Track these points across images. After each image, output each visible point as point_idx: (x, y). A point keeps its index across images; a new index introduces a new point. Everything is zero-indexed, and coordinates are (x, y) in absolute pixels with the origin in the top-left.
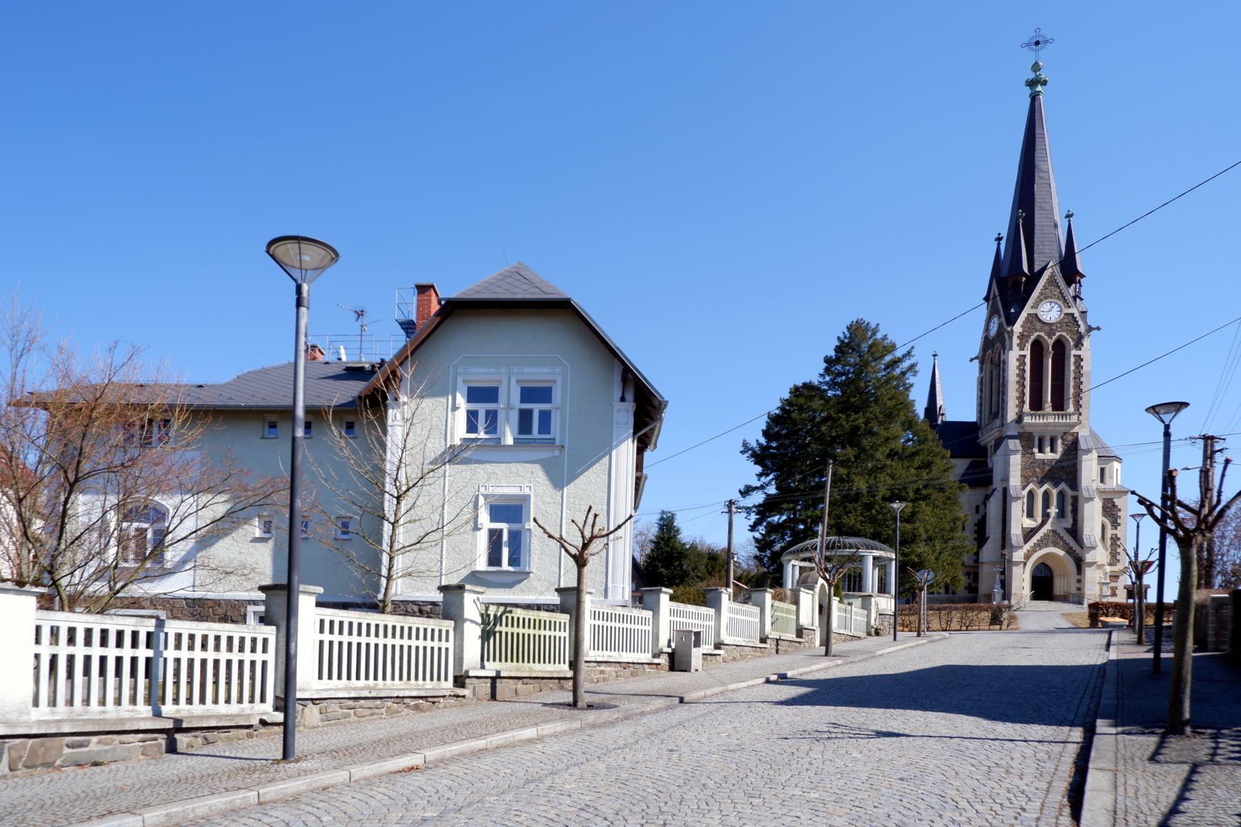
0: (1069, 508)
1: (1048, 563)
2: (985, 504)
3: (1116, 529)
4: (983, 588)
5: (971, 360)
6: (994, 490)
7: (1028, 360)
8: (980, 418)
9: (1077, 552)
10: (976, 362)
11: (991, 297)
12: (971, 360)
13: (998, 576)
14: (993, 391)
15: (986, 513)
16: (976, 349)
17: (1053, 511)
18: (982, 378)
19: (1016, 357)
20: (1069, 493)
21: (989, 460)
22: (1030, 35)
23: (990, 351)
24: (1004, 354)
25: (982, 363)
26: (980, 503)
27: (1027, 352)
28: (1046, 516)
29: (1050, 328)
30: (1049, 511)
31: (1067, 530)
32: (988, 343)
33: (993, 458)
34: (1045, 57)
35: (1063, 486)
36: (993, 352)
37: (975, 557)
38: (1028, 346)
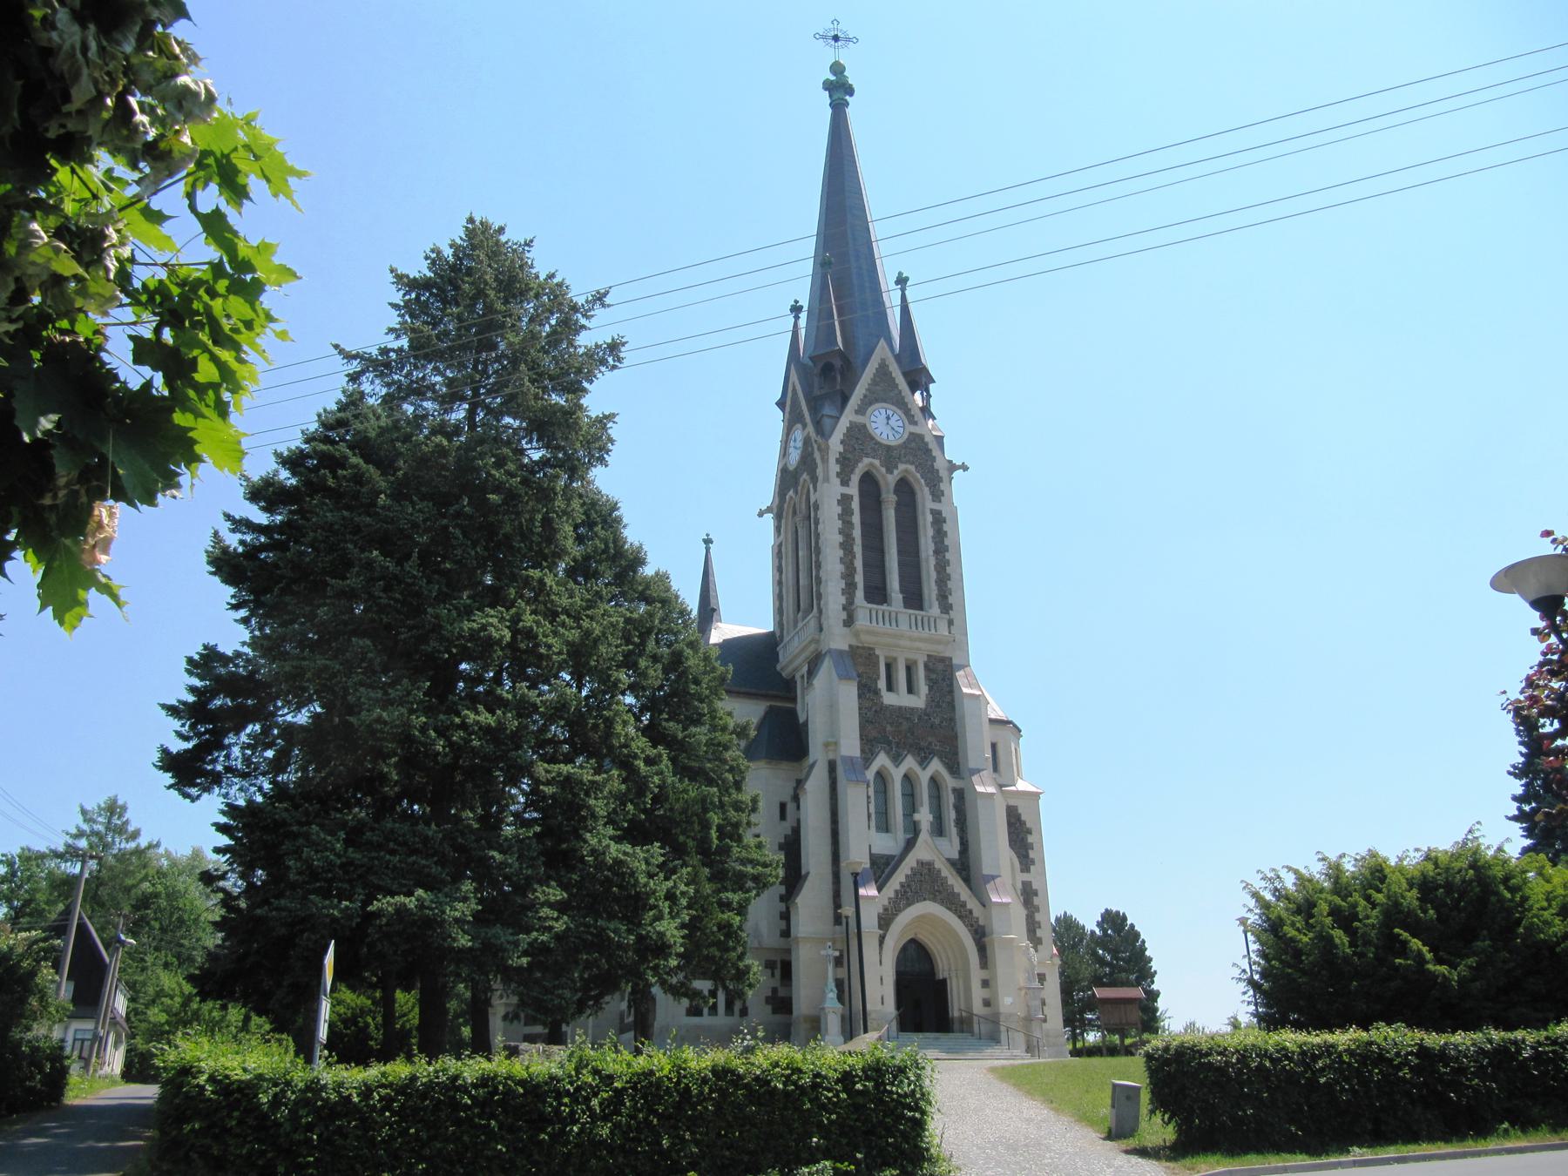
0: (950, 815)
1: (925, 938)
2: (796, 799)
3: (1028, 870)
4: (802, 1002)
5: (761, 514)
6: (812, 766)
7: (855, 505)
8: (780, 623)
9: (976, 914)
10: (769, 517)
11: (788, 403)
12: (761, 514)
13: (830, 968)
14: (801, 567)
15: (799, 821)
16: (767, 495)
17: (924, 816)
18: (780, 546)
19: (831, 493)
20: (950, 782)
21: (799, 707)
22: (824, 26)
23: (791, 493)
24: (815, 490)
25: (779, 517)
26: (787, 798)
27: (853, 490)
28: (914, 830)
29: (890, 455)
30: (917, 817)
31: (952, 862)
32: (788, 479)
33: (807, 698)
34: (845, 56)
35: (936, 766)
36: (796, 492)
37: (783, 923)
38: (855, 479)
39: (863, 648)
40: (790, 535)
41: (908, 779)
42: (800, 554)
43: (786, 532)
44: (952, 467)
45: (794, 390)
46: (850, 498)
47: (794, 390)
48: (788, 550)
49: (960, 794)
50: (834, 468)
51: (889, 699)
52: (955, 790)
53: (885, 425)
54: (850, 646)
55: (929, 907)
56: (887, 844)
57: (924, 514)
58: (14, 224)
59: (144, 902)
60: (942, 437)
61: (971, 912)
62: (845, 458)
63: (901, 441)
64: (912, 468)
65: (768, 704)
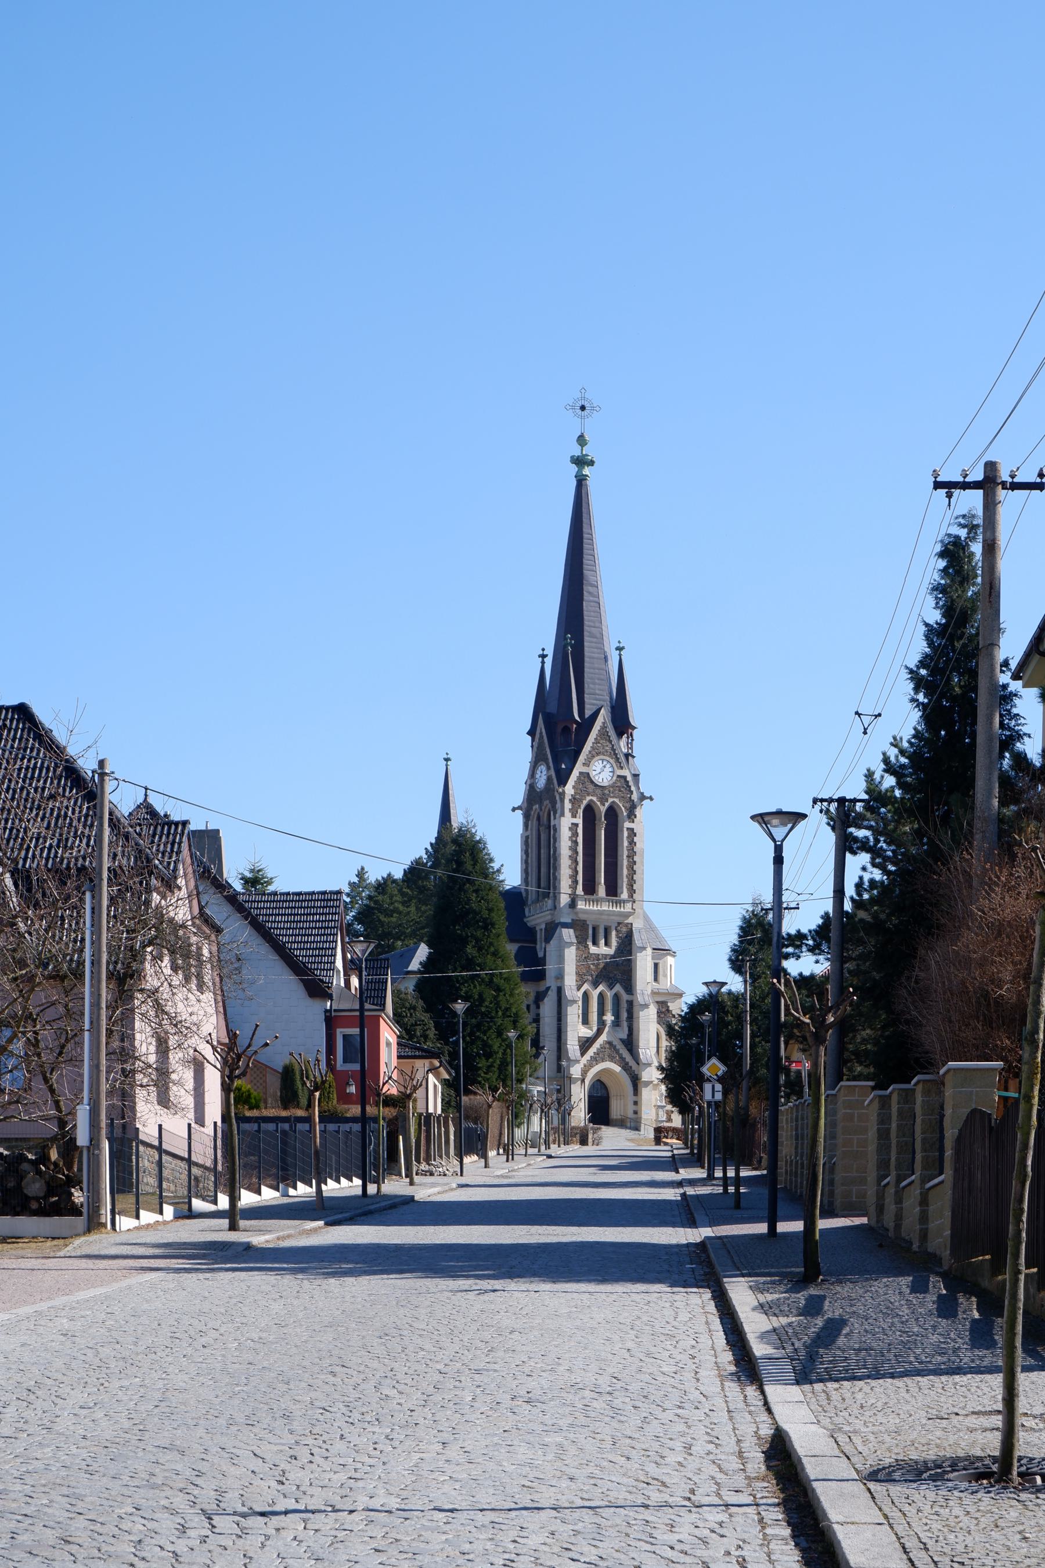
0: (624, 1015)
5: (514, 809)
10: (519, 812)
12: (514, 809)
17: (609, 1018)
18: (527, 837)
20: (625, 997)
25: (527, 817)
27: (579, 821)
28: (602, 1024)
30: (605, 1018)
35: (618, 988)
38: (580, 812)
39: (580, 920)
40: (534, 833)
41: (601, 996)
42: (542, 851)
43: (531, 830)
44: (643, 797)
45: (541, 733)
46: (577, 825)
47: (541, 733)
48: (533, 842)
49: (630, 1004)
50: (568, 805)
51: (593, 949)
52: (627, 1001)
53: (602, 772)
54: (572, 920)
55: (608, 1065)
56: (586, 1032)
57: (622, 831)
58: (844, 1332)
59: (287, 1074)
60: (638, 775)
61: (631, 1067)
62: (574, 799)
63: (611, 782)
64: (617, 800)
65: (519, 945)
